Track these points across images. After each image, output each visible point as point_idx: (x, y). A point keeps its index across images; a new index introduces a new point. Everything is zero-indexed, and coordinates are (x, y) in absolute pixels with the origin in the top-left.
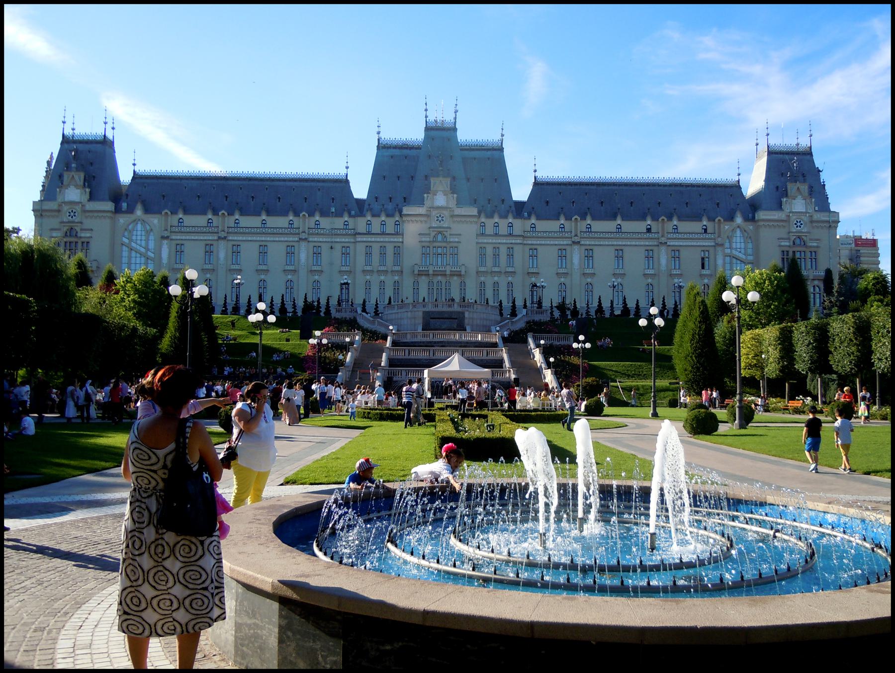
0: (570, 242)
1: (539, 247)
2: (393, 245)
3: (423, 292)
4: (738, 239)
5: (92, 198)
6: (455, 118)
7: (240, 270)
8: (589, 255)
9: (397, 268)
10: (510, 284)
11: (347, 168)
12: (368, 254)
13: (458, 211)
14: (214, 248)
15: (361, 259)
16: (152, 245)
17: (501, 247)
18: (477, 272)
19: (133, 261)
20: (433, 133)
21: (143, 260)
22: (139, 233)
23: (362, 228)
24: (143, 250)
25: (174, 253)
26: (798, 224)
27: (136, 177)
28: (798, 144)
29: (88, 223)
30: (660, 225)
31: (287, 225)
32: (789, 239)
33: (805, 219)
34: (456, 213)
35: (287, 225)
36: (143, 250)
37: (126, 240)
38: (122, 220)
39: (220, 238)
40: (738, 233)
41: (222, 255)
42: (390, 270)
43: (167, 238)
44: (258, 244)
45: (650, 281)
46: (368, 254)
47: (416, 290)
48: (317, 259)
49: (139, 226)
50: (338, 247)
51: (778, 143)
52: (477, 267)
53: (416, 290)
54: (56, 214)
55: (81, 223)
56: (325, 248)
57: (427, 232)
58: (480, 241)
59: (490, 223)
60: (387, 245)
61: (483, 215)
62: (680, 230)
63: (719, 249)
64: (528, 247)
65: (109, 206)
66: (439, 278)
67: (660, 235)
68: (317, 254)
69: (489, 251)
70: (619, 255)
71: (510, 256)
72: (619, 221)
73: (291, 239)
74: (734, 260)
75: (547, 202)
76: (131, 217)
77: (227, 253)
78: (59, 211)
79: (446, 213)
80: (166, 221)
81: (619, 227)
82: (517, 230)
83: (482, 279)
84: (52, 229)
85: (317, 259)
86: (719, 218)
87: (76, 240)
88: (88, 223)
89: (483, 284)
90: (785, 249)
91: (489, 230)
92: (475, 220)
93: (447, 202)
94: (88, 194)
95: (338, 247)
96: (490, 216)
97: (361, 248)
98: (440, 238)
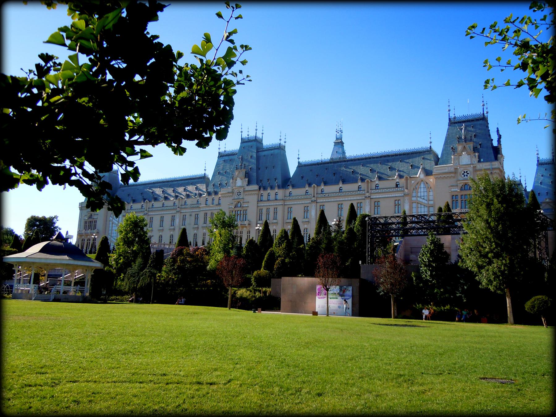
0: (403, 195)
1: (325, 204)
4: (422, 189)
5: (249, 183)
11: (205, 170)
14: (362, 205)
20: (245, 144)
22: (422, 189)
25: (373, 208)
26: (465, 173)
27: (301, 166)
28: (225, 151)
29: (247, 198)
30: (366, 184)
32: (457, 186)
33: (470, 169)
34: (246, 189)
40: (422, 185)
44: (393, 200)
49: (422, 185)
51: (268, 144)
54: (231, 194)
55: (243, 199)
56: (188, 215)
57: (455, 184)
59: (265, 193)
60: (270, 207)
61: (262, 189)
62: (380, 187)
63: (407, 198)
67: (366, 191)
68: (184, 219)
69: (264, 211)
71: (275, 213)
72: (341, 185)
73: (398, 195)
74: (419, 205)
75: (302, 177)
81: (340, 189)
82: (280, 196)
84: (452, 186)
86: (314, 185)
87: (240, 209)
88: (247, 198)
90: (455, 194)
91: (265, 198)
92: (256, 192)
93: (243, 183)
94: (477, 157)
96: (265, 189)
98: (239, 205)
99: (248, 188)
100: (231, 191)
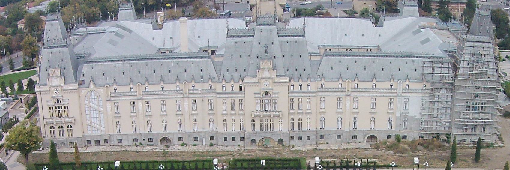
1: (410, 98)
2: (306, 98)
3: (258, 128)
6: (304, 24)
7: (167, 115)
8: (356, 102)
9: (242, 112)
10: (309, 120)
12: (224, 104)
13: (277, 80)
15: (220, 108)
16: (101, 104)
17: (295, 98)
18: (289, 113)
19: (92, 112)
21: (97, 112)
23: (220, 90)
24: (97, 107)
31: (337, 86)
34: (65, 88)
35: (337, 86)
36: (97, 107)
37: (86, 102)
38: (84, 91)
39: (398, 96)
41: (348, 105)
42: (229, 113)
43: (349, 95)
45: (390, 116)
46: (224, 104)
47: (253, 126)
48: (194, 107)
50: (206, 100)
52: (289, 111)
53: (253, 126)
57: (258, 92)
58: (291, 95)
59: (296, 85)
60: (295, 98)
64: (319, 98)
65: (76, 86)
66: (267, 118)
70: (374, 102)
71: (309, 103)
76: (89, 89)
77: (143, 106)
78: (50, 91)
79: (60, 88)
80: (107, 91)
83: (292, 117)
85: (194, 107)
88: (276, 89)
89: (292, 120)
95: (206, 100)
97: (220, 101)
99: (66, 87)
100: (48, 89)
